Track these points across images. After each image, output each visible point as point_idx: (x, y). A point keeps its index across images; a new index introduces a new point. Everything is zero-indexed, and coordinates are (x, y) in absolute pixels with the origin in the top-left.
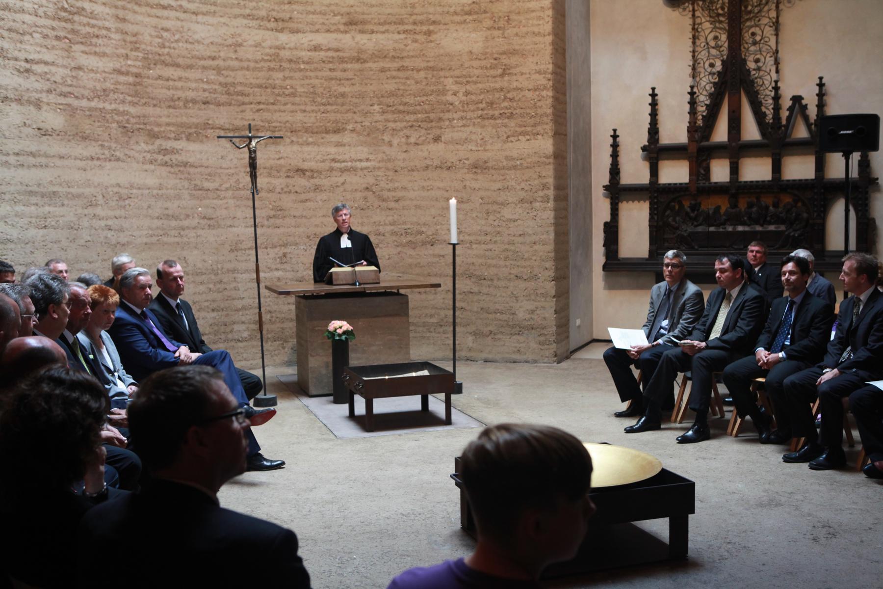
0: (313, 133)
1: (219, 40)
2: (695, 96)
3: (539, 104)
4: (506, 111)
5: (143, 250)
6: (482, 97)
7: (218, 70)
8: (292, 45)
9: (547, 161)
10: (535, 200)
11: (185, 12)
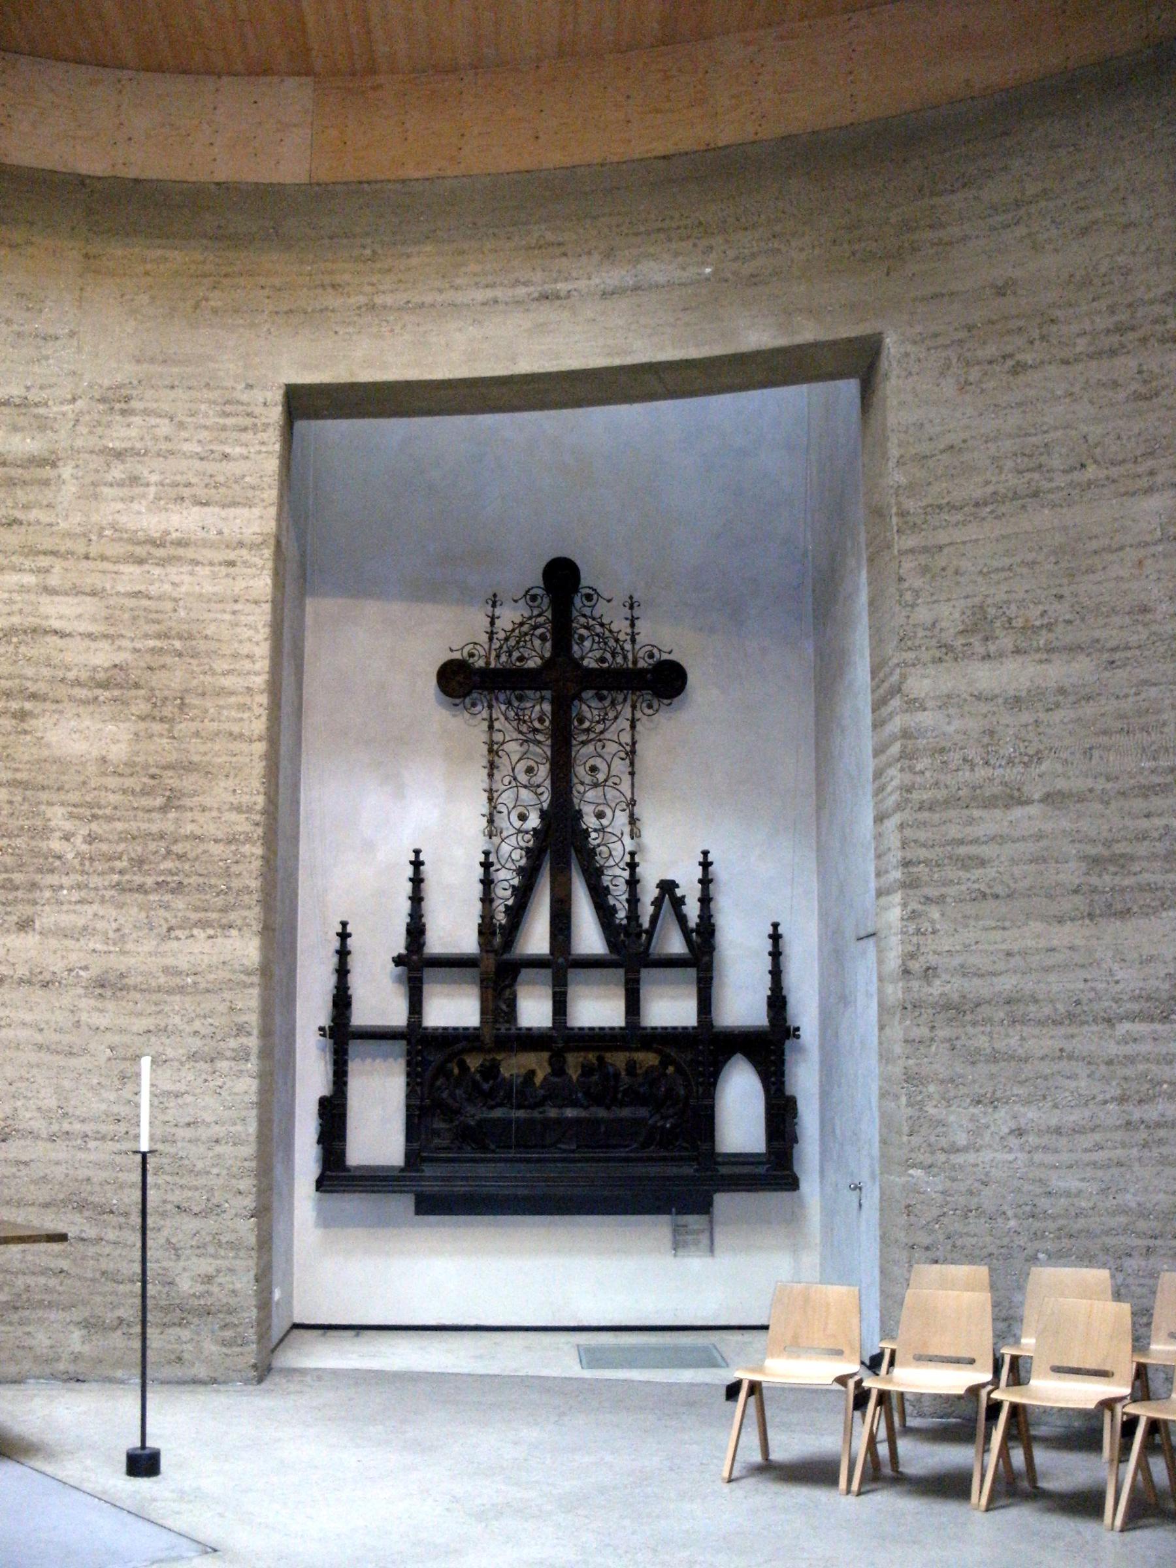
2: (492, 869)
3: (235, 869)
4: (169, 879)
6: (121, 847)
9: (248, 980)
10: (220, 1055)
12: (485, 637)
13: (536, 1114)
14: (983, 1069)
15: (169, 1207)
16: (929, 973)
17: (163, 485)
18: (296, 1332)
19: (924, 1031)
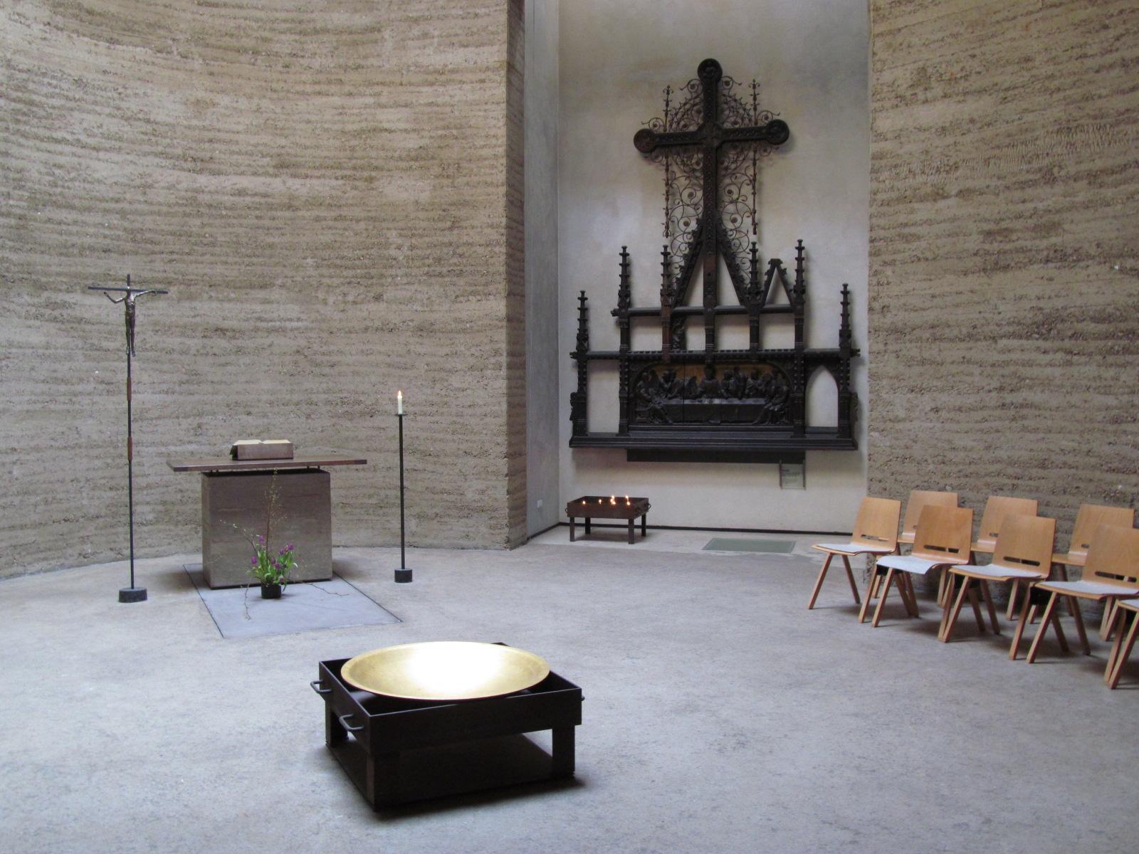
0: (235, 288)
1: (125, 180)
3: (491, 261)
4: (455, 268)
5: (23, 419)
6: (429, 252)
7: (123, 214)
8: (212, 188)
9: (500, 324)
11: (83, 147)
14: (916, 370)
15: (461, 452)
16: (884, 308)
17: (442, 37)
19: (881, 347)
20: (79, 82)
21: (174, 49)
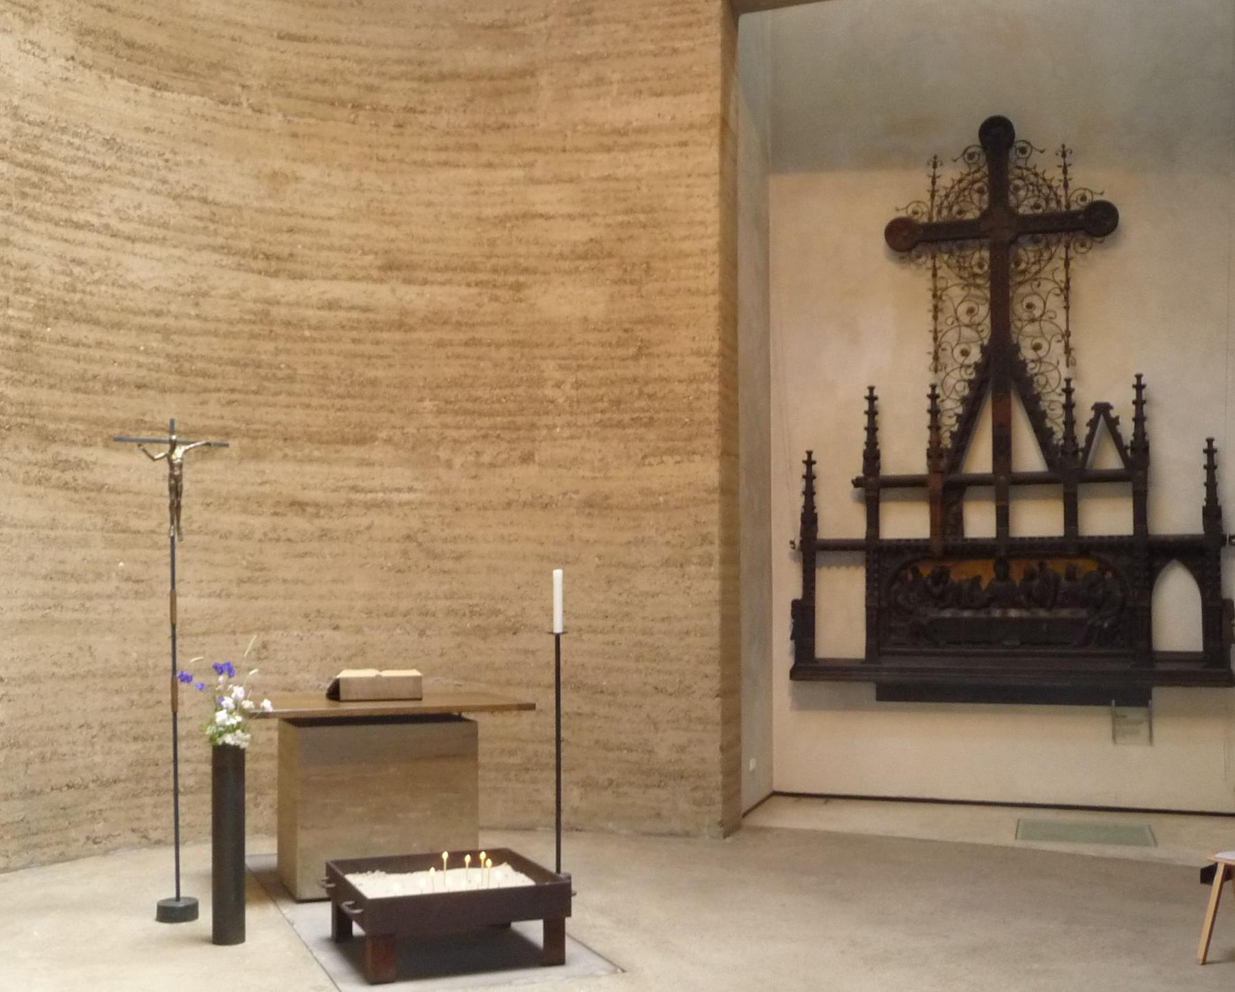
0: (321, 442)
2: (938, 401)
3: (696, 404)
4: (642, 415)
6: (602, 391)
10: (689, 562)
12: (928, 196)
13: (982, 615)
15: (648, 688)
18: (774, 798)
20: (110, 143)
21: (243, 99)
